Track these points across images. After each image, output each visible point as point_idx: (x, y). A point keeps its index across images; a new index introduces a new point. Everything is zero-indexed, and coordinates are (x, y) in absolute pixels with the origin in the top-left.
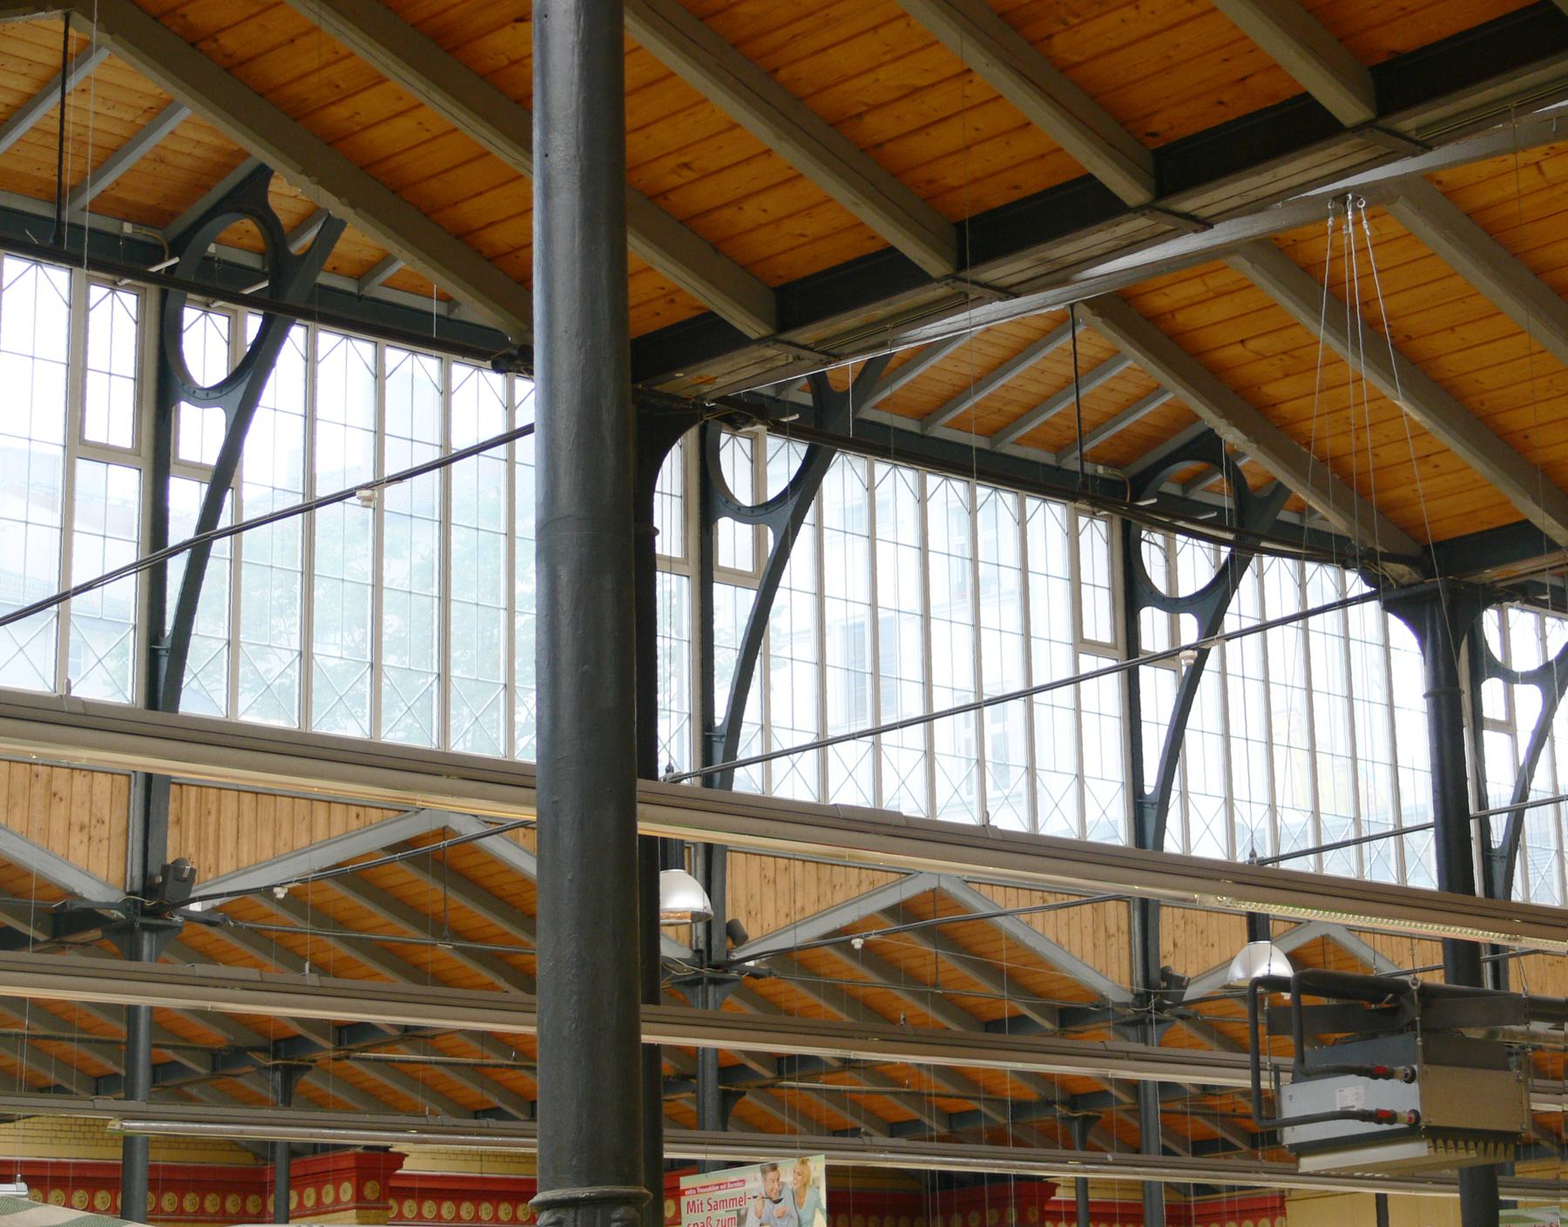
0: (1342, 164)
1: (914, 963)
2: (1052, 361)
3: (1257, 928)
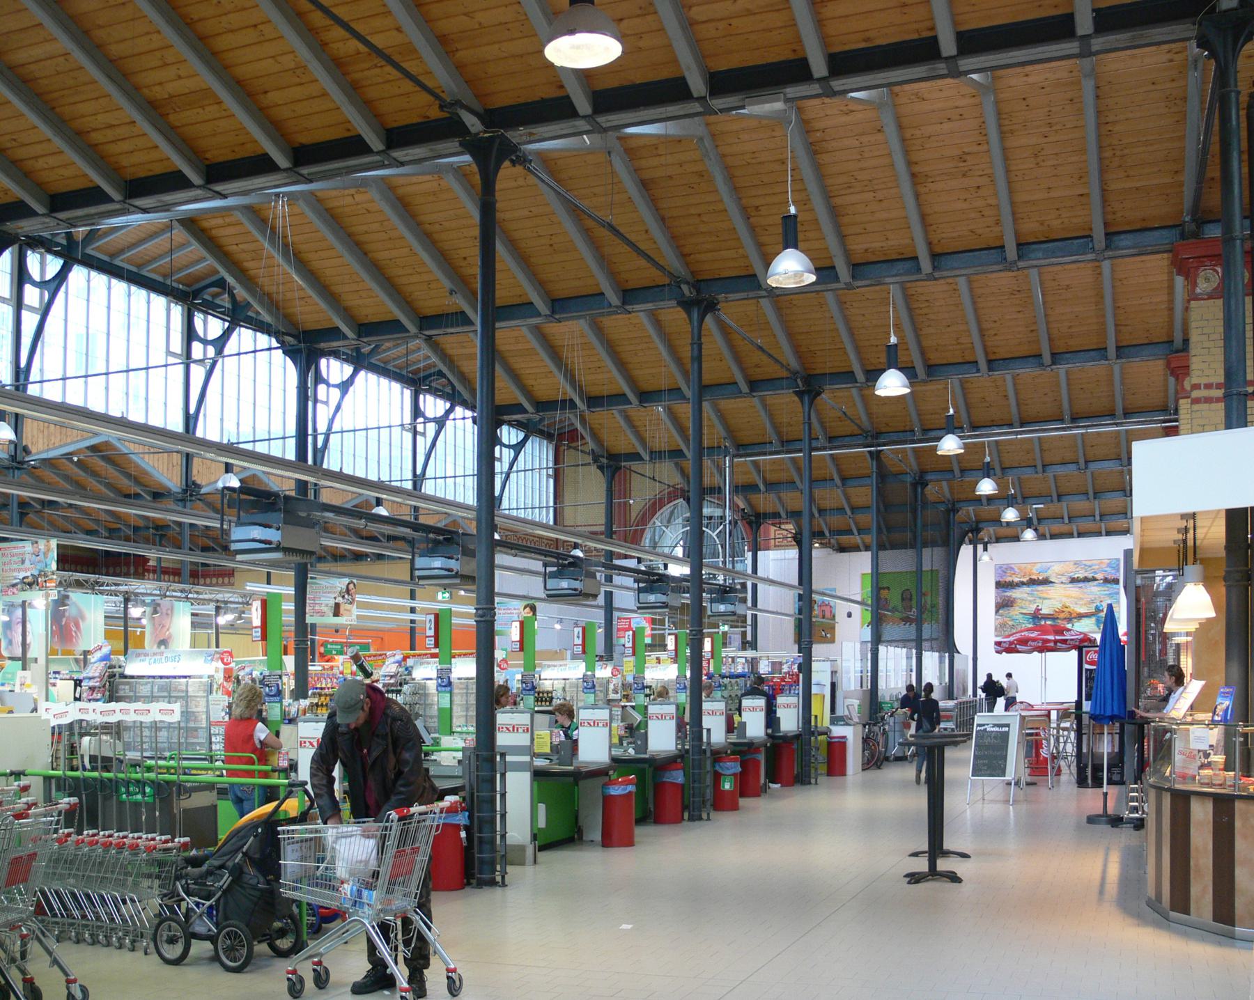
0: (277, 183)
1: (98, 469)
2: (162, 242)
3: (228, 468)
